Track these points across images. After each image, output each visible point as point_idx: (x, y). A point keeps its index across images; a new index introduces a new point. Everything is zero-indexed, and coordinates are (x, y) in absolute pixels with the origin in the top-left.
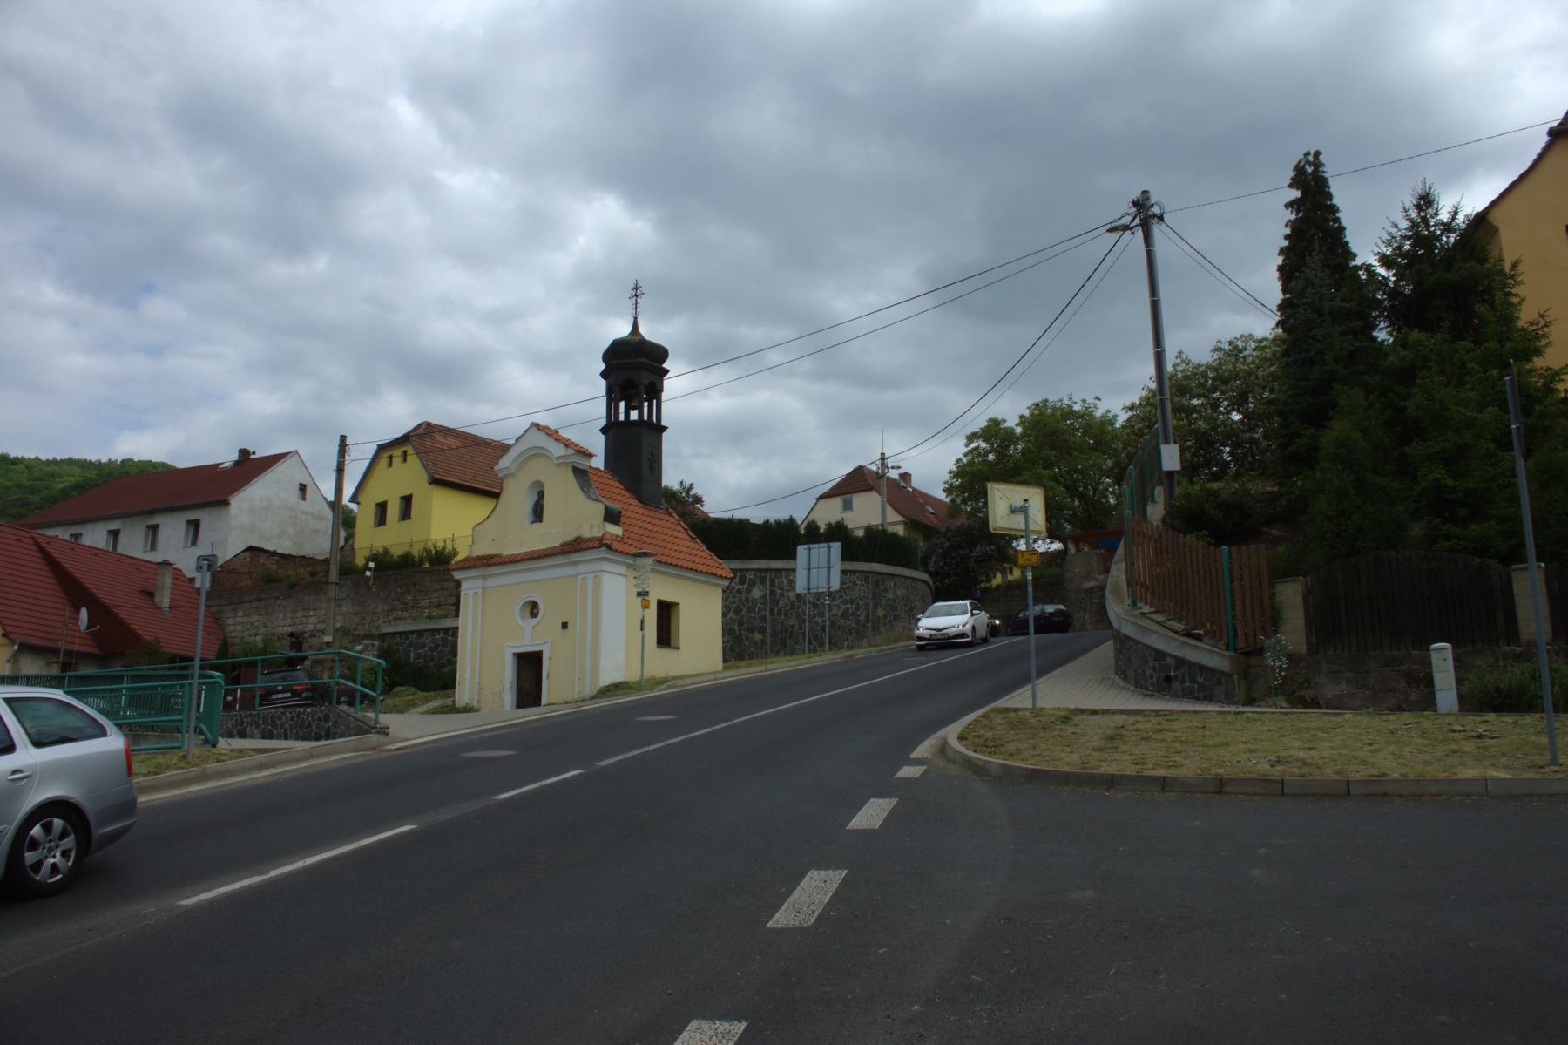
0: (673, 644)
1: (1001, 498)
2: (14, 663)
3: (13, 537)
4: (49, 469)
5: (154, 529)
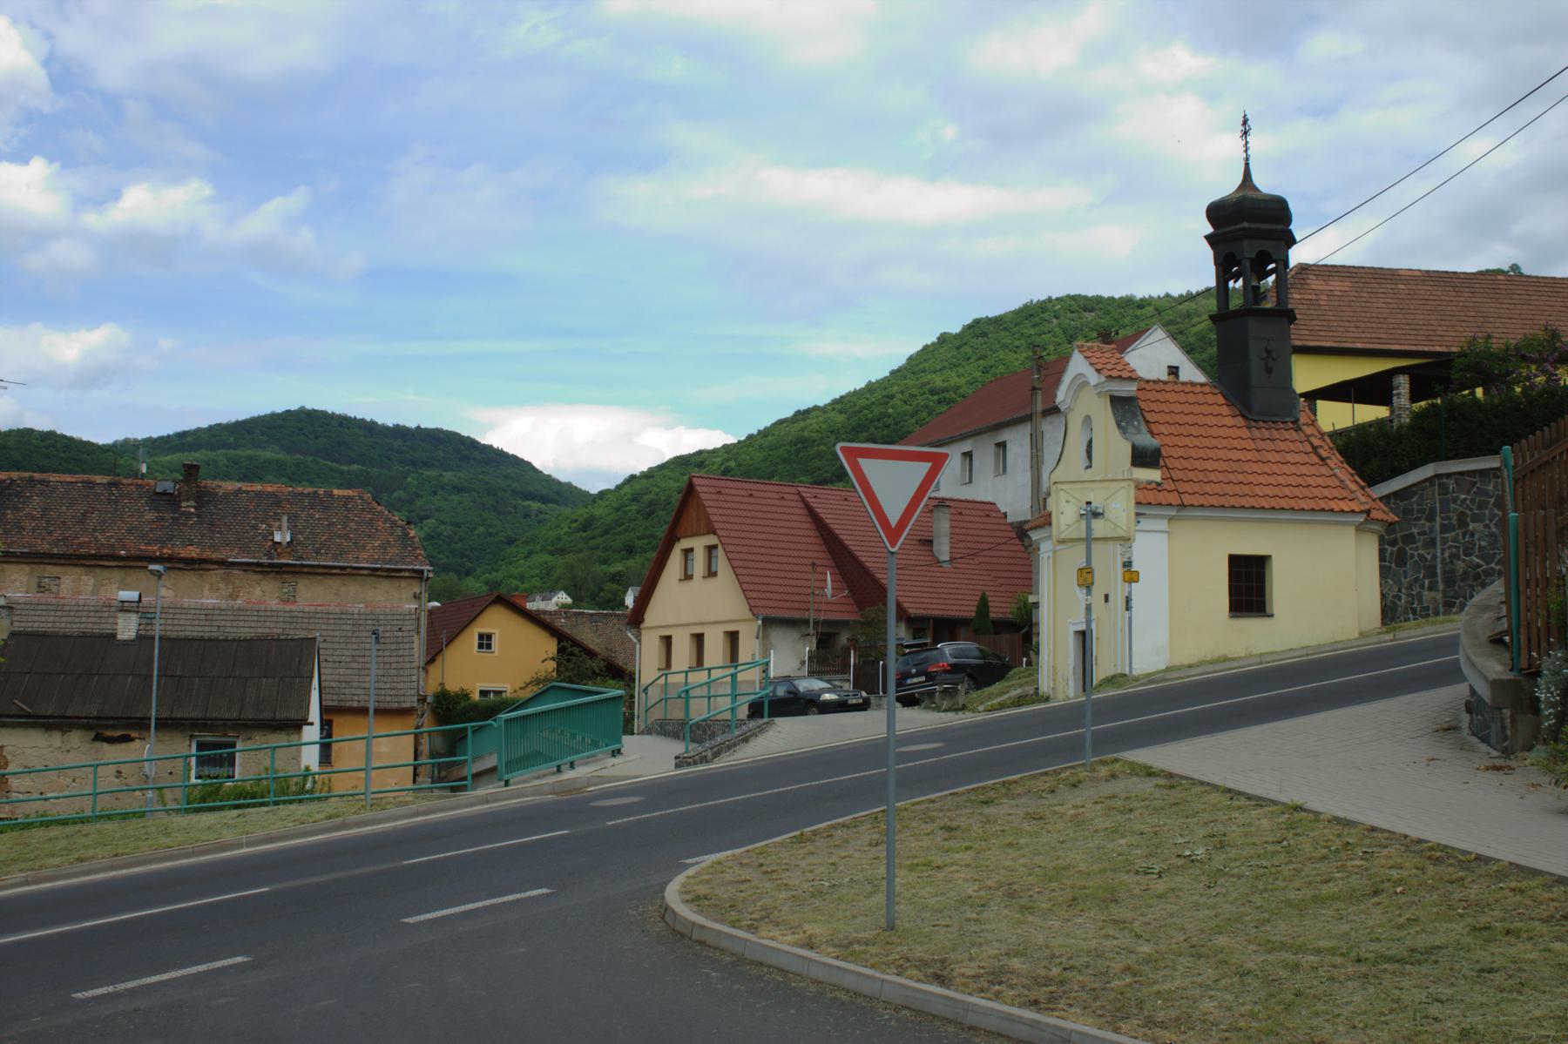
0: (1268, 612)
1: (1067, 502)
2: (764, 638)
3: (774, 495)
4: (1183, 308)
5: (1002, 446)
